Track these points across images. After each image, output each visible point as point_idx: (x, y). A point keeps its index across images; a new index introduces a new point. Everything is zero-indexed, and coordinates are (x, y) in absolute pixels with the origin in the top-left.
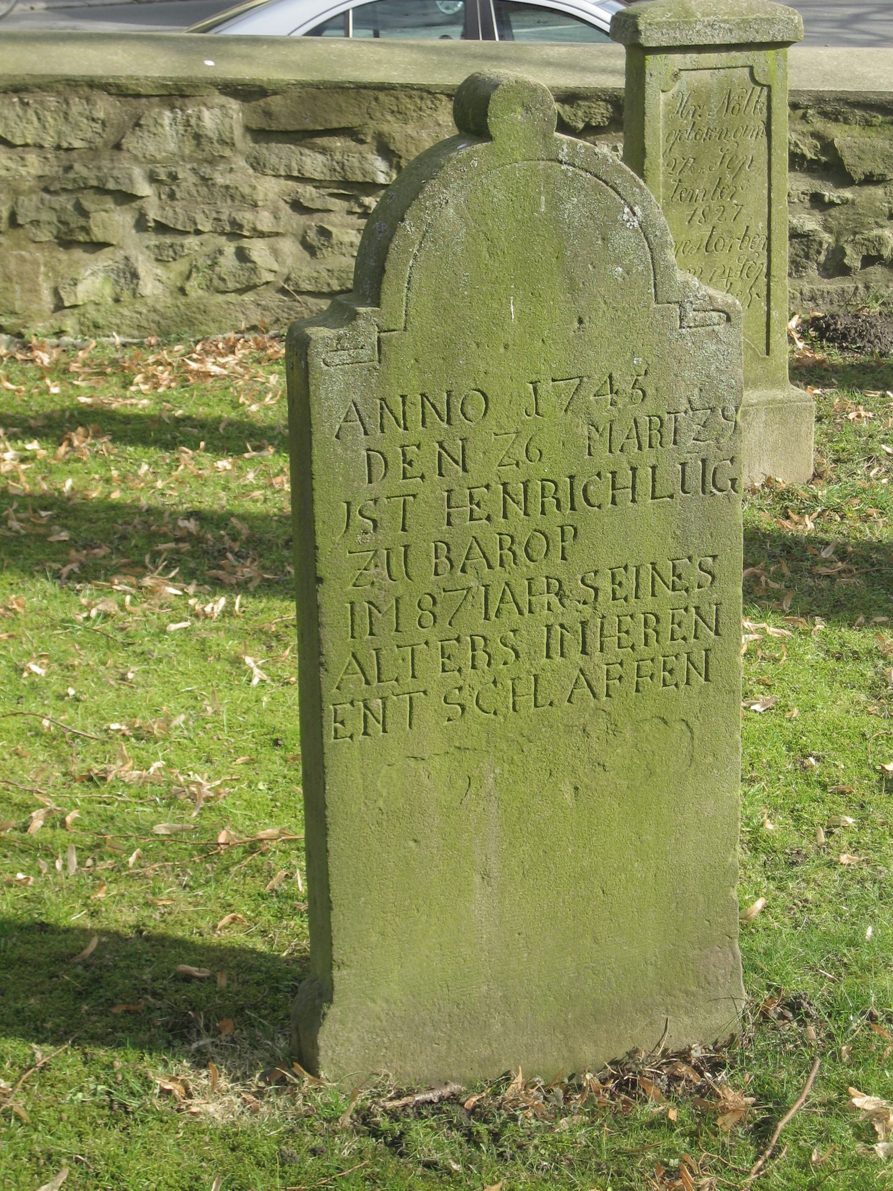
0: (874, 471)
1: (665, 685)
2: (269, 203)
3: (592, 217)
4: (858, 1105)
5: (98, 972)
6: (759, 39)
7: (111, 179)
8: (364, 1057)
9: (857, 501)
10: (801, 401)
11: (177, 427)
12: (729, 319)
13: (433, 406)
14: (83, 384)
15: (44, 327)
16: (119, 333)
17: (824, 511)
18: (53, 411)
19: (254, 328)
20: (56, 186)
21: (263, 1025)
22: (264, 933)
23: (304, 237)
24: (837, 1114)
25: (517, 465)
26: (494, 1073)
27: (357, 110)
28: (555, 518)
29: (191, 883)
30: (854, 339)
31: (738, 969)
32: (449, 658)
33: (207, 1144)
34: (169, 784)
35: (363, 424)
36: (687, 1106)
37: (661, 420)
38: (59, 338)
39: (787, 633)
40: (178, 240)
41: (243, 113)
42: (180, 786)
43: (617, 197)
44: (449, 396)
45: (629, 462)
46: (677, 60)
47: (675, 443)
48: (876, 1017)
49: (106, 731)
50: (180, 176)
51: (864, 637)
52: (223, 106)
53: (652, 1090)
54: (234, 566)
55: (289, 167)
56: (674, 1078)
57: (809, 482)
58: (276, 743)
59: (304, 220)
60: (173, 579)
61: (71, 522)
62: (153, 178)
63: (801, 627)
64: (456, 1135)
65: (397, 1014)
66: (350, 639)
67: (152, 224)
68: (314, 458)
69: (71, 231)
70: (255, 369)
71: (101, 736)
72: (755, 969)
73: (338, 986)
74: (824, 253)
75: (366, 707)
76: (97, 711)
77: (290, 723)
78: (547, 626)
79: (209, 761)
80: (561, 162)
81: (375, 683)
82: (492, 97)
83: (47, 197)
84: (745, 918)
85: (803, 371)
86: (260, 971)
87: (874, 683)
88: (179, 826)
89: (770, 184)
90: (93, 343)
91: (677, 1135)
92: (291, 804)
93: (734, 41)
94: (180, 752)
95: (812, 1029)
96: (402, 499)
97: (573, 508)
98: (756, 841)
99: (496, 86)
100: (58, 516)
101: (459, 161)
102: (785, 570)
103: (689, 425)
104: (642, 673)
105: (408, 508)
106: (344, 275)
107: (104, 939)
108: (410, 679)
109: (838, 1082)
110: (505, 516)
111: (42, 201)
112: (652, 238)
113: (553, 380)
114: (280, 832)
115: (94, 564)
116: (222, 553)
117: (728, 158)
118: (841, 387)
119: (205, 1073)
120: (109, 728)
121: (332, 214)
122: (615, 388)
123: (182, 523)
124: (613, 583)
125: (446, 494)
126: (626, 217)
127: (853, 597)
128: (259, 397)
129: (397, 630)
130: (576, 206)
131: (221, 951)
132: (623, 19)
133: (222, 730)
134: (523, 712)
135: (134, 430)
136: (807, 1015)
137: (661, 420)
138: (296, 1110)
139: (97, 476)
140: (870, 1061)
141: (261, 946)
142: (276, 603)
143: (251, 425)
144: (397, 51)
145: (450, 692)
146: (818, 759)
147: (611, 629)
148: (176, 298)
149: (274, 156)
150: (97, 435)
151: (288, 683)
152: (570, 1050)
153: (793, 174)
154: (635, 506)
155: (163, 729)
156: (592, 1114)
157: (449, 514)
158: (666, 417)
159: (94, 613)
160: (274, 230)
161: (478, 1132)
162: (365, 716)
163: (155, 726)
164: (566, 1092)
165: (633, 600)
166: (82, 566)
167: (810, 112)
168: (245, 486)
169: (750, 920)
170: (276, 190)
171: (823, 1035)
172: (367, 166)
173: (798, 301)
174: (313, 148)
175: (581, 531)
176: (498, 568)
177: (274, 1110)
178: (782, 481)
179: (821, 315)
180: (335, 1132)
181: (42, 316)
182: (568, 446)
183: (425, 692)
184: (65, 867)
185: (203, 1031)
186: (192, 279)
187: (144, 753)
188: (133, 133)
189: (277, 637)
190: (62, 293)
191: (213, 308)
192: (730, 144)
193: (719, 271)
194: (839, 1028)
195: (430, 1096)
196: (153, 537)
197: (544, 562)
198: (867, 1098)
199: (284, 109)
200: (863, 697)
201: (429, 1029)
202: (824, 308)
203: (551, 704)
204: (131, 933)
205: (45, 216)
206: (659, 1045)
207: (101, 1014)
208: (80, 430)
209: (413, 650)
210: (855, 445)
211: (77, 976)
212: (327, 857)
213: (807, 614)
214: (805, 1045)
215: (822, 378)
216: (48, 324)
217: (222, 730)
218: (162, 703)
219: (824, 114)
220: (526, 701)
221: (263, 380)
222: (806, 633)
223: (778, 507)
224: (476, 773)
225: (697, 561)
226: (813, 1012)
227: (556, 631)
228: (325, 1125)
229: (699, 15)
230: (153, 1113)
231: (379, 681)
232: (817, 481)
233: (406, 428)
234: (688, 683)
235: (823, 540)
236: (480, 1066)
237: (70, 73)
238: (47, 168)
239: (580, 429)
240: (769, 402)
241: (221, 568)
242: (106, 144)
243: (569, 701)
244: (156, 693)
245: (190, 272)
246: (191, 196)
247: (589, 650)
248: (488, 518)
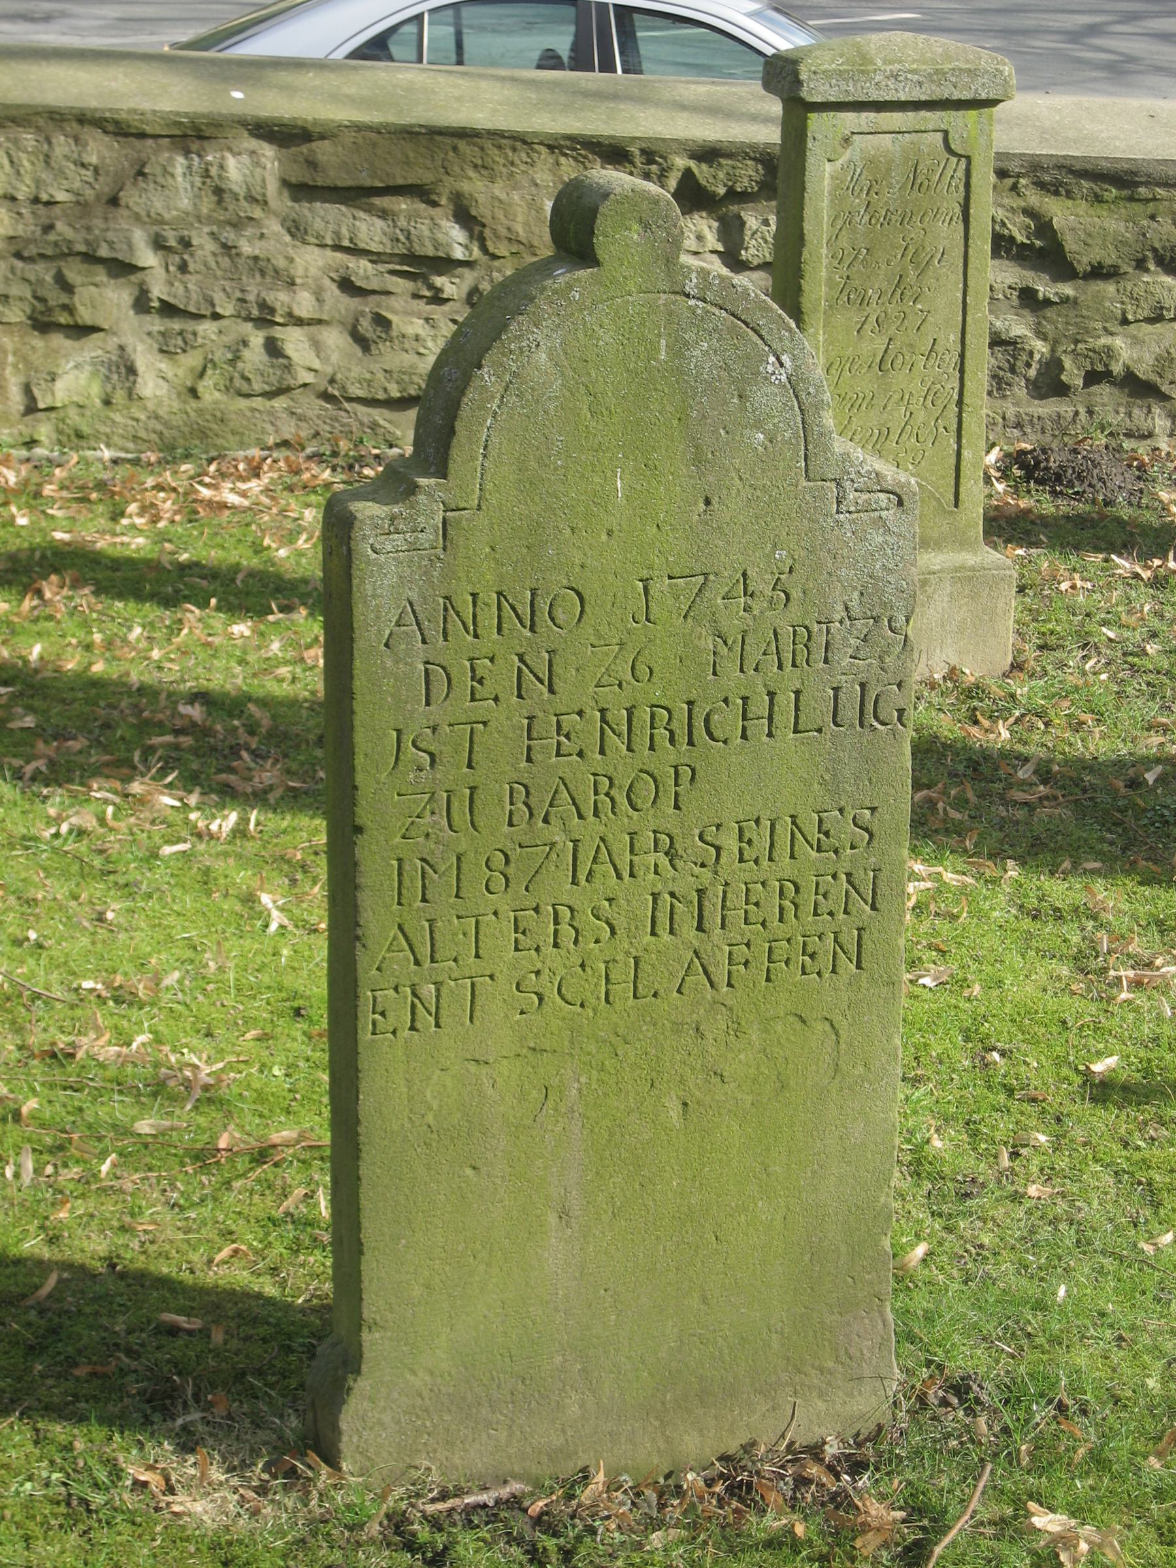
0: (1091, 663)
1: (804, 973)
2: (310, 281)
3: (727, 368)
4: (1038, 1526)
5: (56, 1319)
7: (104, 244)
8: (399, 1444)
9: (1066, 704)
10: (998, 568)
11: (181, 577)
12: (900, 503)
13: (513, 608)
14: (59, 514)
15: (10, 435)
16: (108, 446)
17: (1023, 715)
18: (19, 550)
19: (285, 444)
20: (32, 250)
21: (270, 1396)
22: (274, 1271)
23: (355, 327)
24: (1012, 1537)
25: (620, 686)
26: (568, 1469)
27: (429, 163)
28: (669, 755)
29: (182, 1202)
30: (1070, 481)
31: (889, 1340)
32: (524, 933)
33: (192, 1556)
34: (157, 1065)
35: (420, 629)
36: (818, 1519)
37: (809, 632)
38: (30, 449)
39: (970, 880)
40: (190, 325)
41: (280, 162)
42: (171, 1068)
43: (760, 342)
44: (533, 595)
45: (765, 685)
46: (850, 119)
47: (826, 661)
48: (1067, 1407)
49: (76, 990)
50: (194, 242)
51: (1069, 888)
52: (253, 153)
53: (772, 1496)
54: (249, 769)
55: (337, 234)
56: (802, 1481)
57: (1005, 675)
58: (297, 1012)
60: (170, 786)
61: (37, 703)
62: (158, 244)
63: (988, 873)
64: (516, 1551)
65: (444, 1390)
66: (395, 907)
67: (156, 304)
68: (355, 672)
69: (50, 310)
70: (286, 499)
71: (71, 997)
72: (911, 1338)
73: (367, 1353)
74: (1035, 366)
75: (414, 994)
76: (66, 963)
77: (315, 987)
78: (653, 894)
79: (209, 1034)
80: (688, 296)
81: (427, 963)
82: (601, 209)
83: (19, 264)
84: (901, 1268)
85: (1003, 523)
86: (268, 1323)
87: (1080, 952)
88: (167, 1123)
90: (75, 458)
91: (803, 1560)
92: (315, 1097)
93: (923, 98)
94: (172, 1022)
95: (982, 1421)
96: (468, 727)
97: (691, 743)
98: (919, 1162)
99: (606, 196)
100: (21, 694)
101: (555, 292)
102: (970, 795)
103: (845, 638)
104: (774, 957)
105: (476, 739)
107: (66, 1275)
108: (472, 959)
109: (1013, 1493)
110: (602, 752)
111: (13, 270)
112: (803, 395)
113: (670, 578)
114: (300, 1135)
115: (67, 762)
116: (235, 751)
117: (912, 250)
118: (1052, 547)
119: (192, 1460)
120: (80, 987)
121: (393, 298)
122: (750, 589)
123: (185, 709)
124: (741, 840)
125: (526, 722)
126: (770, 369)
127: (1057, 833)
128: (290, 538)
129: (457, 896)
130: (705, 353)
131: (217, 1294)
132: (780, 63)
133: (228, 993)
134: (618, 1005)
135: (125, 579)
136: (978, 1401)
137: (809, 632)
138: (310, 1512)
139: (74, 641)
140: (1057, 1466)
141: (270, 1290)
142: (304, 821)
143: (279, 577)
144: (484, 84)
145: (524, 977)
146: (1003, 1054)
147: (737, 900)
148: (185, 402)
149: (318, 220)
150: (76, 585)
151: (316, 931)
152: (668, 1441)
153: (997, 262)
154: (772, 741)
155: (151, 989)
156: (694, 1527)
157: (529, 748)
158: (815, 628)
159: (64, 828)
160: (317, 316)
161: (545, 1548)
162: (413, 1006)
163: (141, 987)
164: (660, 1496)
165: (765, 863)
166: (52, 763)
167: (1023, 181)
168: (268, 659)
169: (907, 1271)
170: (320, 264)
171: (997, 1428)
172: (440, 236)
173: (999, 428)
174: (369, 210)
175: (700, 773)
176: (591, 818)
177: (280, 1514)
178: (970, 674)
179: (1029, 447)
180: (359, 1544)
181: (8, 420)
182: (687, 662)
183: (491, 977)
184: (17, 1175)
185: (191, 1402)
186: (206, 378)
187: (125, 1023)
188: (135, 184)
189: (304, 867)
190: (36, 392)
191: (234, 417)
192: (915, 233)
193: (896, 397)
194: (1018, 1419)
195: (483, 1498)
196: (145, 727)
197: (652, 812)
198: (1051, 1516)
199: (333, 158)
200: (1065, 971)
201: (485, 1411)
202: (1032, 437)
203: (655, 995)
204: (100, 1267)
205: (15, 290)
206: (783, 1436)
207: (59, 1376)
208: (54, 578)
209: (477, 922)
210: (1067, 626)
211: (29, 1324)
212: (358, 1187)
213: (997, 855)
214: (972, 1441)
215: (1027, 533)
216: (15, 431)
217: (228, 993)
218: (150, 954)
219: (1041, 185)
220: (623, 990)
221: (295, 515)
222: (994, 881)
223: (964, 708)
224: (555, 1082)
225: (850, 814)
226: (984, 1397)
227: (665, 901)
228: (347, 1534)
229: (879, 63)
230: (123, 1512)
231: (432, 961)
232: (1016, 673)
233: (476, 636)
234: (834, 971)
235: (1021, 754)
236: (551, 1459)
237: (53, 103)
238: (20, 227)
239: (703, 641)
241: (232, 770)
242: (98, 198)
243: (679, 991)
244: (142, 940)
245: (205, 368)
246: (209, 269)
247: (706, 925)
248: (580, 754)
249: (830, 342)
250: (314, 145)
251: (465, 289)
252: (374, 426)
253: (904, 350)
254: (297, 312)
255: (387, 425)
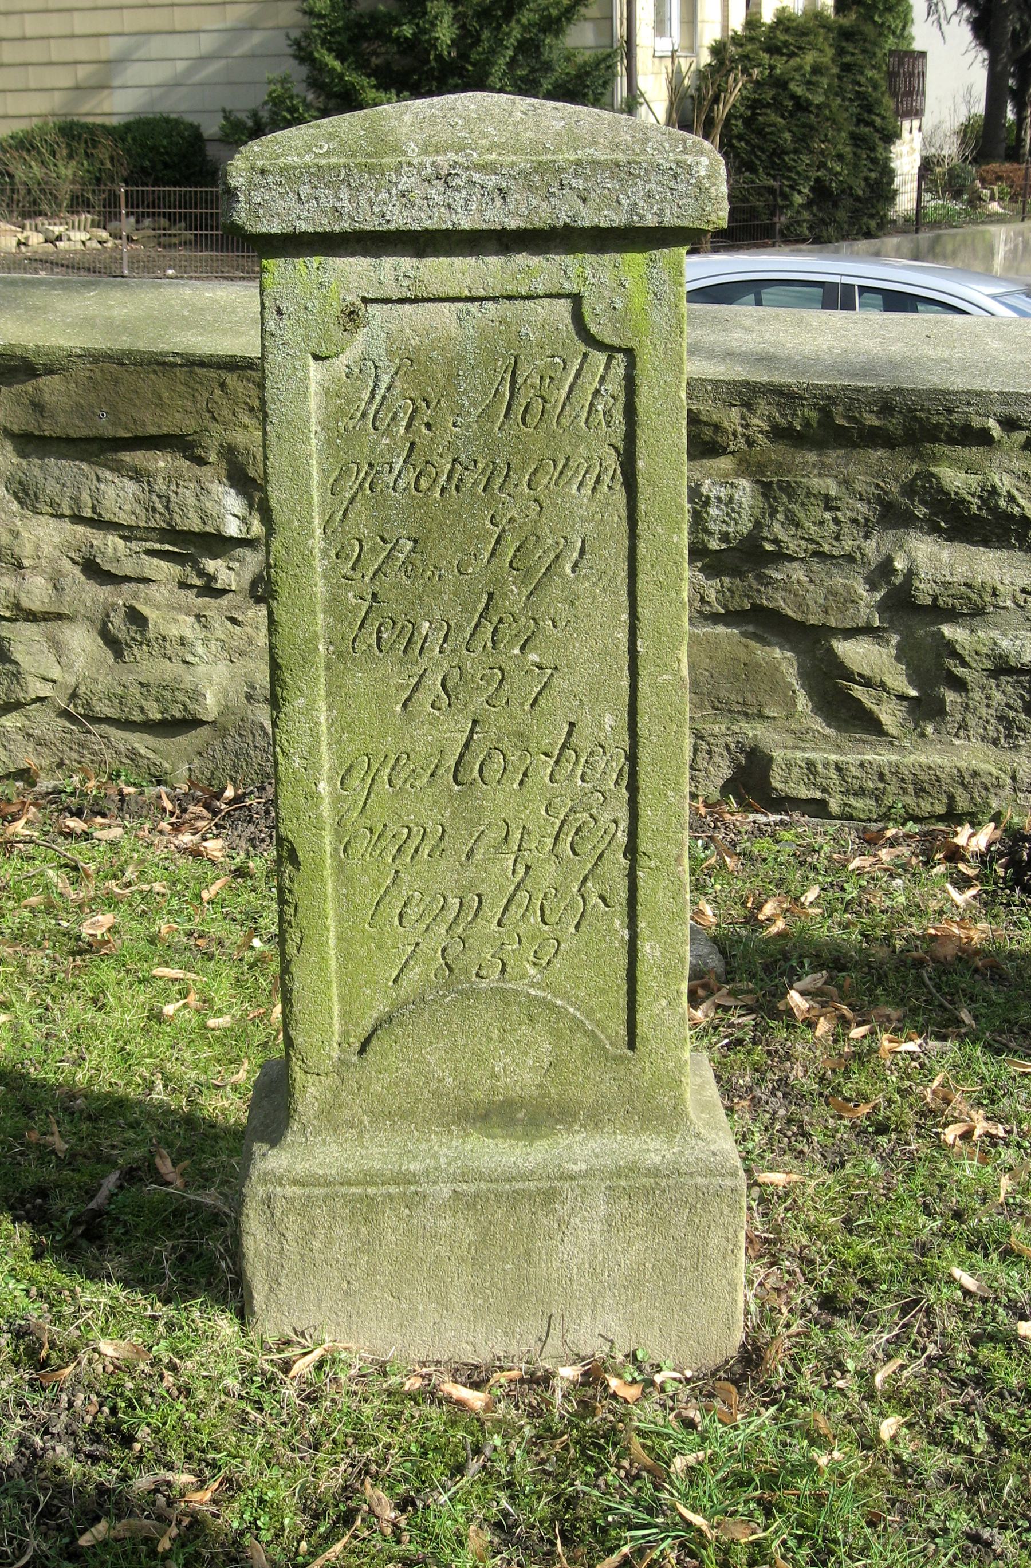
6: (588, 218)
23: (104, 624)
46: (354, 272)
55: (76, 500)
59: (104, 593)
89: (634, 616)
93: (512, 223)
106: (167, 694)
121: (153, 587)
160: (52, 610)
170: (56, 540)
174: (117, 468)
193: (494, 835)
199: (65, 399)
229: (413, 150)
240: (619, 1172)
249: (342, 725)
250: (41, 380)
251: (248, 577)
252: (133, 755)
253: (506, 744)
254: (26, 603)
255: (152, 755)
